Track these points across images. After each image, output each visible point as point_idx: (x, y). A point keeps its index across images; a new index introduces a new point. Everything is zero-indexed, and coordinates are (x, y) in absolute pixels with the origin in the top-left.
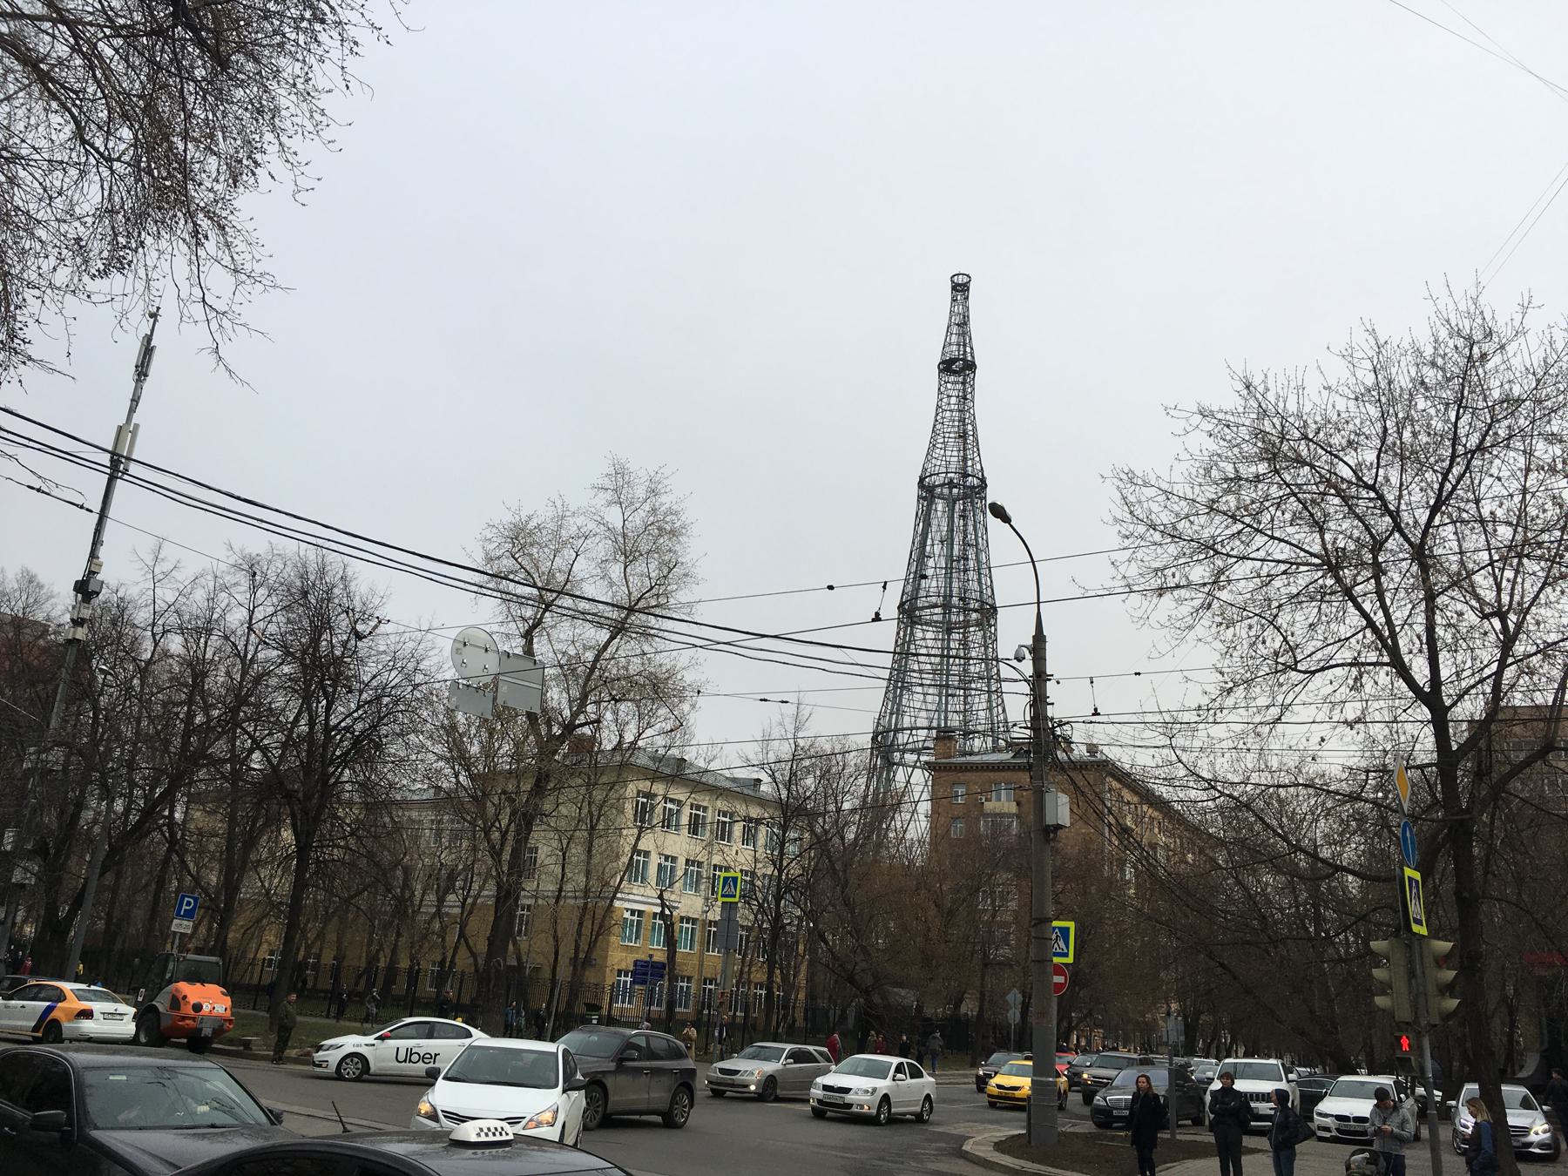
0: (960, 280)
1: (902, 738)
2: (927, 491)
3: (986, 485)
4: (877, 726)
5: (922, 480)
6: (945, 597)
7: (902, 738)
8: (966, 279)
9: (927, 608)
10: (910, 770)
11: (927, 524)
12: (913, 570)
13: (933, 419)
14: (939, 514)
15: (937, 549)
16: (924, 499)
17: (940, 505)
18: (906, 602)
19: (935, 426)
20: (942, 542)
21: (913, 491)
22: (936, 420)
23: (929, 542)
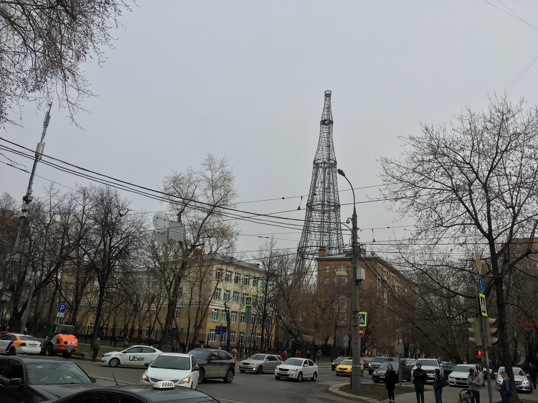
0: (328, 93)
1: (308, 250)
2: (316, 165)
3: (337, 163)
4: (299, 246)
5: (314, 161)
6: (322, 201)
7: (308, 250)
12: (312, 192)
14: (321, 173)
15: (320, 185)
16: (315, 168)
17: (321, 170)
19: (319, 143)
20: (321, 183)
21: (312, 165)
22: (320, 141)
23: (317, 183)
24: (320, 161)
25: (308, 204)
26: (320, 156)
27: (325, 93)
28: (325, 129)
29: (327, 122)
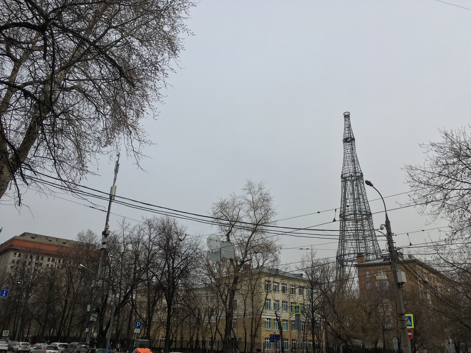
0: (347, 114)
1: (346, 257)
2: (344, 179)
5: (342, 176)
7: (346, 257)
8: (348, 114)
10: (350, 267)
11: (345, 189)
12: (343, 204)
13: (343, 157)
14: (349, 185)
15: (350, 196)
16: (344, 181)
17: (349, 183)
20: (351, 194)
21: (340, 179)
23: (347, 195)
24: (347, 175)
27: (344, 115)
28: (348, 146)
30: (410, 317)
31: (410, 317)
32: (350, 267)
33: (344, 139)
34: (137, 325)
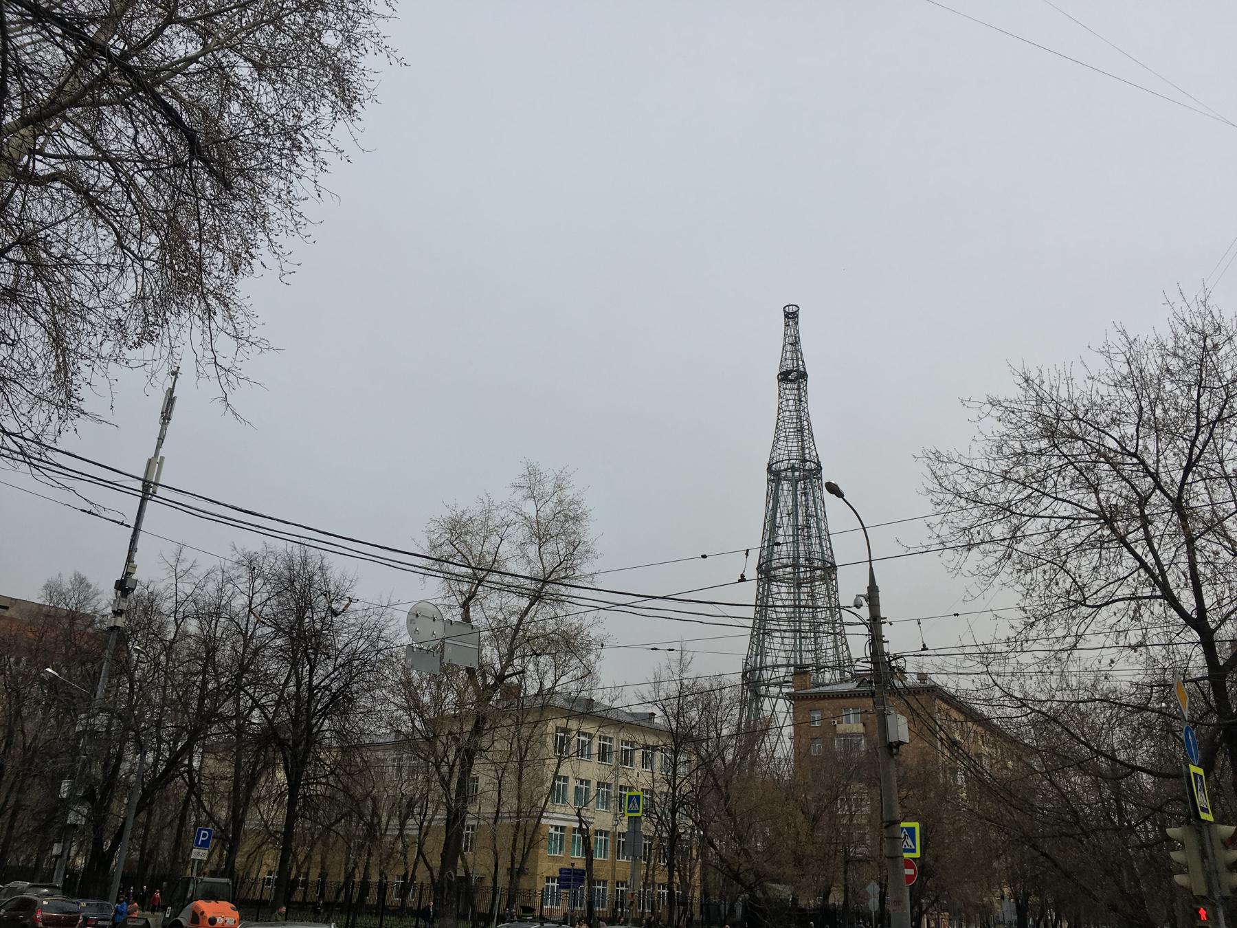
0: (791, 309)
1: (767, 674)
2: (775, 475)
4: (746, 665)
5: (770, 466)
6: (793, 558)
7: (767, 674)
8: (795, 309)
9: (780, 568)
11: (776, 501)
12: (767, 538)
15: (785, 520)
16: (773, 481)
17: (785, 486)
18: (763, 564)
19: (777, 423)
20: (789, 514)
21: (764, 475)
23: (778, 515)
24: (783, 466)
25: (760, 566)
26: (782, 454)
27: (785, 311)
28: (791, 393)
29: (793, 377)
30: (914, 829)
31: (914, 829)
32: (774, 700)
33: (781, 374)
34: (201, 839)
